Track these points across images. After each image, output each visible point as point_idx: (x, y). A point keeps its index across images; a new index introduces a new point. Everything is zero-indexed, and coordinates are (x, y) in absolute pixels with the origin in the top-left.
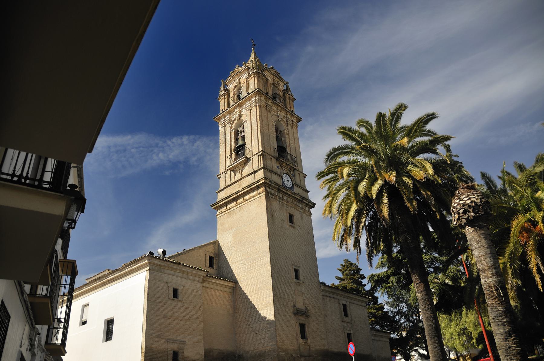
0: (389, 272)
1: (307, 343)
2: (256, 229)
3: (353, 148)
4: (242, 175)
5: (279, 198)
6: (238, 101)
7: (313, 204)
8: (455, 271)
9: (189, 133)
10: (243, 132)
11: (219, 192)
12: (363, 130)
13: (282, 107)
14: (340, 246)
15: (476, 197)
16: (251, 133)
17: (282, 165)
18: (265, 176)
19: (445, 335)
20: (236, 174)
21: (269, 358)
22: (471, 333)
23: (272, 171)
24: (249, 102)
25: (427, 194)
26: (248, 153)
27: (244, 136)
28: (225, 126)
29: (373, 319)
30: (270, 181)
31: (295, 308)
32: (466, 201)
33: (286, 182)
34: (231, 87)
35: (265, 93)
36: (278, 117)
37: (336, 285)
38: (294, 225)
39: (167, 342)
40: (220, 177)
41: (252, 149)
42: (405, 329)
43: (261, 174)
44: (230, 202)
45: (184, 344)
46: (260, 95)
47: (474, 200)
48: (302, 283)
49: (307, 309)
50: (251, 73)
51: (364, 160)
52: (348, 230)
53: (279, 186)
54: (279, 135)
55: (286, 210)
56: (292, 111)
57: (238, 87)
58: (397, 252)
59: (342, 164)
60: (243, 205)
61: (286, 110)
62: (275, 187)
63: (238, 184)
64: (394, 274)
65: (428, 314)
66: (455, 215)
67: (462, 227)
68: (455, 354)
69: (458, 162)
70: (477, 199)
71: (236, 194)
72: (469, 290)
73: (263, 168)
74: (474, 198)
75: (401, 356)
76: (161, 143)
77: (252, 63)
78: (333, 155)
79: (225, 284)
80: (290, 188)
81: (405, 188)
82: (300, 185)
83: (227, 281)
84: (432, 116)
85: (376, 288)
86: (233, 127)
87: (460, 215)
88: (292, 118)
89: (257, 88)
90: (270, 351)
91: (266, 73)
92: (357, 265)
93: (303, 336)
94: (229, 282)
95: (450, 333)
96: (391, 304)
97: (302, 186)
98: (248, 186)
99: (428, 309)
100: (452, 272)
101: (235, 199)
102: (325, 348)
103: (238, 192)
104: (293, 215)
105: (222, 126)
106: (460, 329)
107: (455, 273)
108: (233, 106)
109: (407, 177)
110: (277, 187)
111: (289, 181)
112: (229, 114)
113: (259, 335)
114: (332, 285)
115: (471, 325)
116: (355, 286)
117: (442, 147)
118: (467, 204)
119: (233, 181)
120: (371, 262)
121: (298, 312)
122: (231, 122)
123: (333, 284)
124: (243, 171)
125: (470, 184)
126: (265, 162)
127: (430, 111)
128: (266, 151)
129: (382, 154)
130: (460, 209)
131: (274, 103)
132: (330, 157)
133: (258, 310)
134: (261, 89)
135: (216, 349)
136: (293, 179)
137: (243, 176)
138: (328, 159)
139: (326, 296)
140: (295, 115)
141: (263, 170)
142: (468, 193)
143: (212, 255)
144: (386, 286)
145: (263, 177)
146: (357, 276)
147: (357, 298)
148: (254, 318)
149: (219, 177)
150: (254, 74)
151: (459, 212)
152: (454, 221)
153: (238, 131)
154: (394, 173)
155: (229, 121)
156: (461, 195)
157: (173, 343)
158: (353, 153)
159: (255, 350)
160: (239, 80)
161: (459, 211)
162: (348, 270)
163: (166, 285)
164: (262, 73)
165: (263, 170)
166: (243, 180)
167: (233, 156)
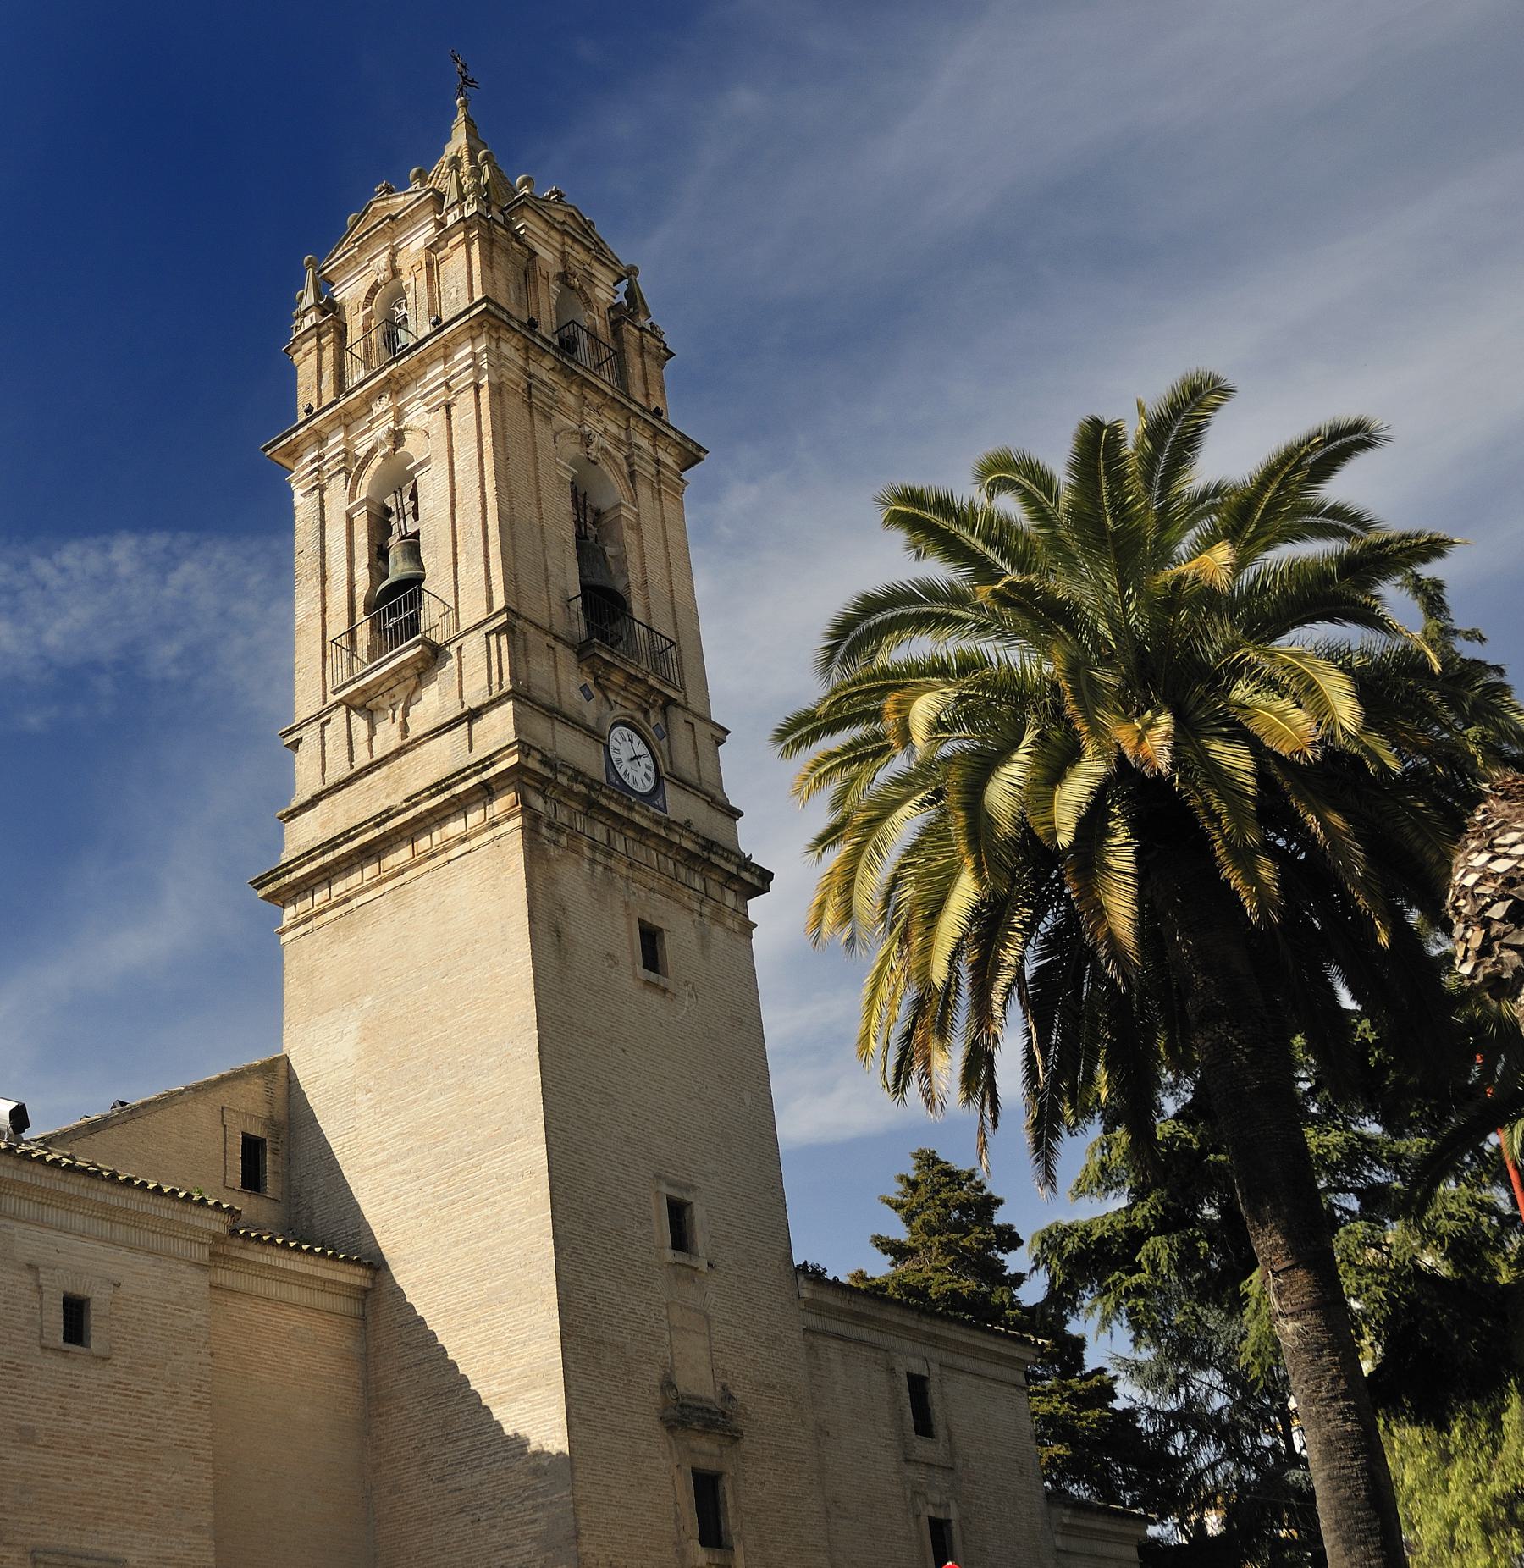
0: (1141, 1212)
3: (958, 598)
4: (405, 728)
5: (593, 848)
6: (389, 364)
8: (1468, 1210)
9: (142, 524)
10: (410, 519)
11: (292, 815)
12: (1009, 506)
13: (607, 394)
14: (896, 1085)
17: (607, 683)
19: (1418, 1529)
20: (379, 728)
23: (553, 713)
25: (1326, 826)
26: (436, 619)
28: (322, 489)
30: (546, 762)
31: (672, 1394)
33: (627, 765)
34: (351, 292)
35: (521, 324)
36: (586, 440)
37: (873, 1279)
40: (299, 741)
41: (457, 603)
42: (1219, 1499)
43: (499, 727)
44: (345, 865)
46: (497, 329)
48: (704, 1267)
49: (731, 1397)
50: (450, 220)
51: (1014, 656)
53: (592, 784)
55: (626, 905)
56: (657, 413)
57: (389, 292)
58: (1177, 1117)
60: (409, 882)
62: (568, 792)
63: (388, 777)
64: (1163, 1226)
65: (1332, 1424)
66: (1466, 929)
69: (1484, 664)
71: (378, 825)
73: (513, 695)
77: (458, 171)
78: (859, 630)
79: (319, 1272)
80: (648, 797)
81: (1220, 796)
82: (695, 782)
83: (334, 1257)
84: (1352, 438)
85: (1076, 1294)
87: (1493, 932)
88: (654, 446)
92: (977, 1179)
94: (341, 1266)
95: (1442, 1517)
96: (1147, 1371)
97: (706, 787)
98: (435, 785)
99: (1335, 1399)
100: (1450, 1216)
103: (388, 814)
104: (661, 930)
105: (307, 485)
106: (1495, 1500)
107: (1467, 1218)
108: (361, 384)
109: (1228, 738)
110: (582, 789)
111: (643, 761)
113: (494, 1527)
114: (854, 1277)
116: (968, 1284)
117: (1405, 591)
119: (362, 759)
120: (1048, 1164)
121: (686, 1412)
122: (352, 466)
123: (861, 1276)
126: (523, 664)
127: (1346, 414)
128: (524, 611)
130: (1493, 902)
131: (567, 373)
133: (485, 1402)
134: (502, 303)
136: (660, 750)
137: (412, 735)
138: (833, 649)
139: (824, 1333)
141: (509, 705)
143: (257, 1131)
144: (1125, 1284)
145: (513, 739)
146: (982, 1236)
147: (979, 1343)
149: (290, 739)
150: (468, 230)
152: (1462, 962)
153: (388, 512)
155: (344, 460)
156: (1498, 832)
158: (960, 621)
160: (393, 256)
162: (936, 1206)
163: (28, 1277)
165: (509, 705)
166: (410, 755)
167: (363, 634)
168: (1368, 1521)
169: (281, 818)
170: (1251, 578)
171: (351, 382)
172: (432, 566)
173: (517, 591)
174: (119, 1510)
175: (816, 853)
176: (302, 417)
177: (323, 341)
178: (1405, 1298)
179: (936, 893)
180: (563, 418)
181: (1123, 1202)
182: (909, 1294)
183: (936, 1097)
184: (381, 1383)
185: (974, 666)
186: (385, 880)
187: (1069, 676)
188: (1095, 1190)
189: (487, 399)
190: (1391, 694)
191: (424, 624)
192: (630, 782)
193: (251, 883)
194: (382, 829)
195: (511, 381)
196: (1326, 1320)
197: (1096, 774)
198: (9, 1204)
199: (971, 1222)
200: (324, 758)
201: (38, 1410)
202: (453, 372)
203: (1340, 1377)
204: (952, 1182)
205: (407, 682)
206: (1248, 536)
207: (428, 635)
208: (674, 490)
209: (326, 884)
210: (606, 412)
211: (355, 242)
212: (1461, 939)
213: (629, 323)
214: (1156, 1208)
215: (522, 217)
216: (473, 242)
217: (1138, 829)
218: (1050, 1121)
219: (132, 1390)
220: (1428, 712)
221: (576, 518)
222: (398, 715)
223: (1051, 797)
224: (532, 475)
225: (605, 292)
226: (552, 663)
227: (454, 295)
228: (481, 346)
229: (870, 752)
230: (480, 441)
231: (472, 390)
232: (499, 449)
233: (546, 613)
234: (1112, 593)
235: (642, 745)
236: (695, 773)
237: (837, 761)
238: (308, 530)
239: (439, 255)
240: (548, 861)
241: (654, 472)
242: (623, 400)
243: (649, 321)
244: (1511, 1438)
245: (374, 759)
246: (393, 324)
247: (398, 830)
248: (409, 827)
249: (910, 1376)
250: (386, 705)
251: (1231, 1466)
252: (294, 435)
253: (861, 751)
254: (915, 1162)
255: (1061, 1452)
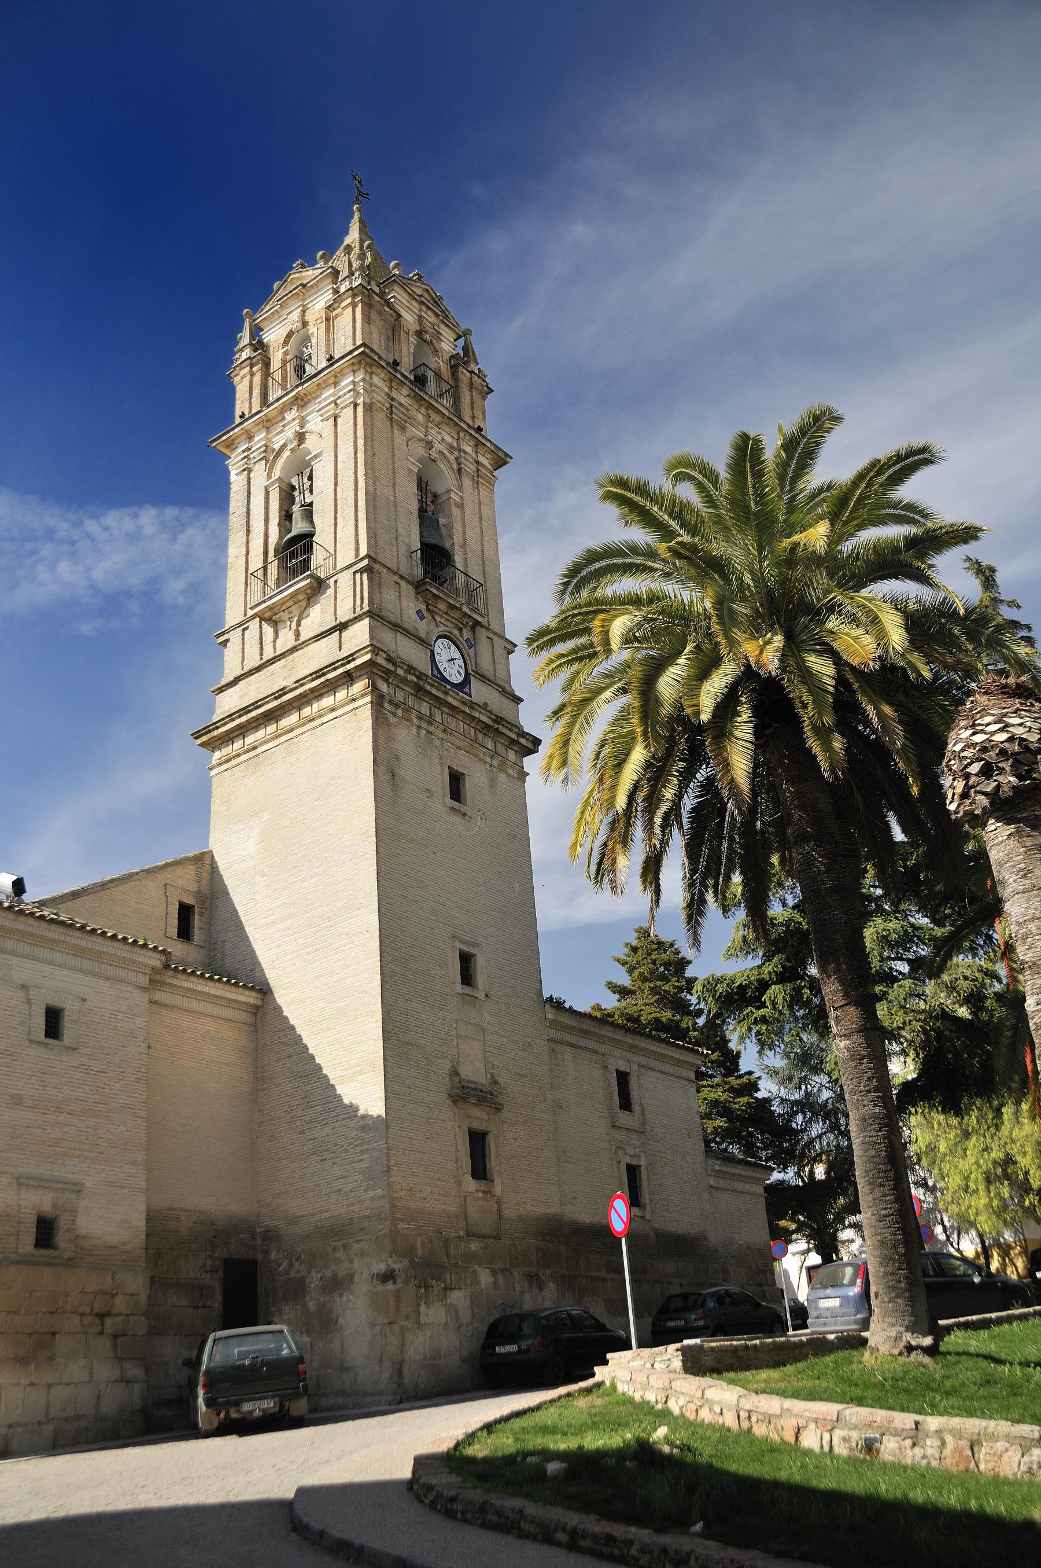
0: (768, 969)
1: (491, 1193)
2: (337, 815)
3: (651, 554)
4: (297, 634)
5: (420, 718)
6: (297, 387)
7: (532, 742)
8: (977, 974)
9: (161, 500)
10: (307, 493)
11: (221, 690)
12: (688, 493)
13: (444, 415)
14: (596, 878)
15: (1028, 724)
16: (336, 494)
17: (434, 609)
18: (375, 643)
19: (946, 1179)
20: (281, 633)
21: (361, 1240)
22: (1027, 1173)
23: (396, 627)
24: (332, 391)
25: (880, 714)
26: (321, 561)
27: (311, 504)
28: (249, 470)
29: (721, 1122)
30: (389, 659)
31: (456, 1079)
32: (994, 733)
33: (446, 664)
34: (274, 335)
35: (388, 363)
36: (429, 445)
37: (606, 1009)
38: (463, 808)
39: (19, 1185)
40: (227, 641)
41: (335, 551)
42: (824, 1157)
43: (359, 635)
44: (254, 725)
45: (79, 1192)
46: (371, 366)
47: (1019, 731)
48: (482, 996)
49: (496, 1082)
50: (343, 289)
51: (686, 595)
52: (621, 825)
53: (421, 676)
54: (431, 508)
55: (441, 757)
56: (479, 429)
57: (300, 337)
58: (794, 908)
59: (610, 604)
60: (296, 737)
61: (456, 424)
62: (404, 681)
63: (285, 666)
64: (782, 978)
65: (867, 1108)
66: (954, 780)
67: (978, 821)
68: (978, 1240)
69: (1019, 623)
70: (1029, 731)
71: (276, 698)
72: (1008, 1034)
73: (370, 614)
74: (1021, 725)
75: (808, 1243)
76: (63, 528)
77: (349, 255)
78: (584, 573)
79: (226, 994)
80: (460, 687)
81: (809, 691)
82: (492, 678)
83: (236, 984)
84: (920, 457)
85: (724, 1021)
86: (276, 474)
87: (971, 783)
88: (476, 452)
89: (361, 342)
90: (368, 1217)
91: (397, 295)
92: (676, 947)
93: (480, 1171)
94: (241, 990)
95: (961, 1173)
96: (781, 1075)
97: (498, 681)
98: (315, 673)
99: (869, 1091)
100: (966, 978)
101: (272, 717)
102: (552, 1211)
103: (283, 691)
104: (464, 774)
105: (239, 467)
106: (995, 1163)
107: (977, 980)
108: (278, 400)
109: (820, 653)
110: (414, 678)
111: (456, 662)
112: (264, 427)
113: (335, 1164)
114: (593, 1008)
115: (1029, 1149)
116: (666, 1015)
117: (971, 573)
118: (996, 746)
119: (269, 654)
120: (695, 934)
121: (466, 1091)
122: (270, 456)
123: (598, 1007)
124: (303, 622)
125: (1013, 681)
126: (378, 593)
127: (917, 442)
128: (380, 558)
129: (748, 579)
130: (972, 762)
131: (418, 399)
132: (575, 581)
133: (332, 1082)
134: (376, 348)
135: (190, 1211)
136: (469, 655)
137: (302, 639)
138: (566, 584)
139: (562, 1042)
140: (488, 444)
141: (367, 621)
142: (1003, 709)
143: (189, 900)
144: (755, 1015)
145: (368, 643)
146: (677, 984)
147: (665, 1052)
148: (320, 1109)
149: (221, 639)
150: (354, 296)
151: (968, 770)
152: (951, 803)
153: (293, 488)
154: (779, 640)
155: (265, 451)
156: (978, 716)
157: (37, 1187)
158: (652, 570)
159: (320, 1212)
160: (304, 312)
161: (966, 767)
162: (648, 963)
163: (21, 994)
164: (382, 295)
165: (367, 621)
166: (300, 652)
167: (273, 569)
168: (886, 1172)
169: (213, 692)
170: (850, 549)
171: (271, 399)
172: (321, 525)
173: (376, 545)
174: (79, 1150)
175: (551, 721)
176: (238, 420)
177: (254, 369)
178: (934, 1030)
179: (623, 750)
180: (414, 429)
181: (758, 962)
182: (628, 1020)
183: (618, 885)
184: (266, 1068)
185: (658, 599)
186: (281, 735)
187: (717, 606)
188: (739, 953)
189: (362, 414)
190: (930, 628)
191: (314, 564)
192: (447, 676)
193: (192, 735)
194: (279, 701)
195: (379, 402)
196: (866, 1040)
197: (730, 674)
198: (9, 944)
199: (671, 974)
200: (243, 653)
201: (25, 1083)
202: (340, 394)
203: (873, 1078)
204: (659, 948)
205: (300, 603)
206: (844, 519)
207: (315, 572)
208: (487, 482)
209: (241, 737)
210: (444, 427)
211: (278, 301)
212: (950, 787)
213: (463, 367)
214: (777, 967)
215: (393, 290)
216: (357, 305)
217: (757, 712)
218: (698, 905)
219: (92, 1070)
220: (952, 643)
221: (420, 498)
222: (294, 625)
223: (698, 688)
224: (391, 467)
225: (447, 345)
226: (398, 594)
227: (343, 342)
228: (359, 377)
229: (585, 656)
230: (355, 442)
231: (352, 407)
232: (368, 448)
233: (395, 560)
234: (754, 556)
235: (457, 651)
236: (492, 672)
237: (565, 660)
238: (239, 498)
239: (334, 313)
240: (388, 725)
241: (474, 469)
242: (455, 419)
243: (478, 367)
244: (1006, 1123)
245: (276, 654)
246: (302, 359)
247: (290, 702)
248: (298, 700)
249: (618, 1072)
250: (286, 619)
251: (832, 1136)
252: (232, 433)
253: (581, 654)
254: (636, 934)
255: (721, 1124)
